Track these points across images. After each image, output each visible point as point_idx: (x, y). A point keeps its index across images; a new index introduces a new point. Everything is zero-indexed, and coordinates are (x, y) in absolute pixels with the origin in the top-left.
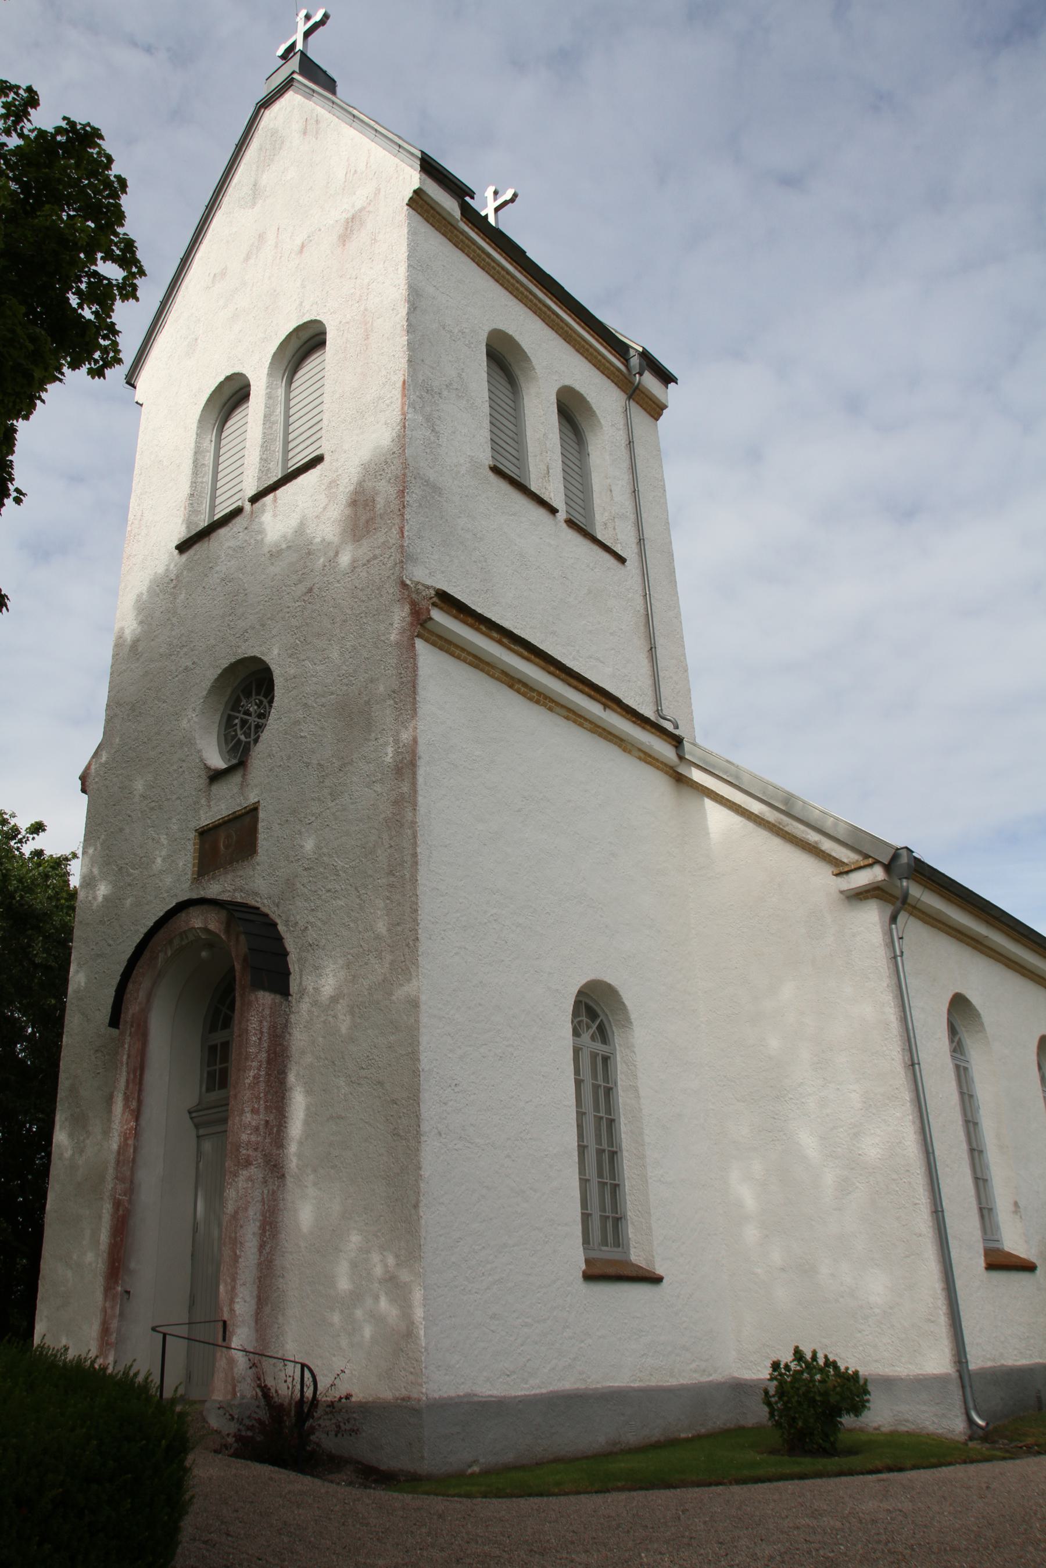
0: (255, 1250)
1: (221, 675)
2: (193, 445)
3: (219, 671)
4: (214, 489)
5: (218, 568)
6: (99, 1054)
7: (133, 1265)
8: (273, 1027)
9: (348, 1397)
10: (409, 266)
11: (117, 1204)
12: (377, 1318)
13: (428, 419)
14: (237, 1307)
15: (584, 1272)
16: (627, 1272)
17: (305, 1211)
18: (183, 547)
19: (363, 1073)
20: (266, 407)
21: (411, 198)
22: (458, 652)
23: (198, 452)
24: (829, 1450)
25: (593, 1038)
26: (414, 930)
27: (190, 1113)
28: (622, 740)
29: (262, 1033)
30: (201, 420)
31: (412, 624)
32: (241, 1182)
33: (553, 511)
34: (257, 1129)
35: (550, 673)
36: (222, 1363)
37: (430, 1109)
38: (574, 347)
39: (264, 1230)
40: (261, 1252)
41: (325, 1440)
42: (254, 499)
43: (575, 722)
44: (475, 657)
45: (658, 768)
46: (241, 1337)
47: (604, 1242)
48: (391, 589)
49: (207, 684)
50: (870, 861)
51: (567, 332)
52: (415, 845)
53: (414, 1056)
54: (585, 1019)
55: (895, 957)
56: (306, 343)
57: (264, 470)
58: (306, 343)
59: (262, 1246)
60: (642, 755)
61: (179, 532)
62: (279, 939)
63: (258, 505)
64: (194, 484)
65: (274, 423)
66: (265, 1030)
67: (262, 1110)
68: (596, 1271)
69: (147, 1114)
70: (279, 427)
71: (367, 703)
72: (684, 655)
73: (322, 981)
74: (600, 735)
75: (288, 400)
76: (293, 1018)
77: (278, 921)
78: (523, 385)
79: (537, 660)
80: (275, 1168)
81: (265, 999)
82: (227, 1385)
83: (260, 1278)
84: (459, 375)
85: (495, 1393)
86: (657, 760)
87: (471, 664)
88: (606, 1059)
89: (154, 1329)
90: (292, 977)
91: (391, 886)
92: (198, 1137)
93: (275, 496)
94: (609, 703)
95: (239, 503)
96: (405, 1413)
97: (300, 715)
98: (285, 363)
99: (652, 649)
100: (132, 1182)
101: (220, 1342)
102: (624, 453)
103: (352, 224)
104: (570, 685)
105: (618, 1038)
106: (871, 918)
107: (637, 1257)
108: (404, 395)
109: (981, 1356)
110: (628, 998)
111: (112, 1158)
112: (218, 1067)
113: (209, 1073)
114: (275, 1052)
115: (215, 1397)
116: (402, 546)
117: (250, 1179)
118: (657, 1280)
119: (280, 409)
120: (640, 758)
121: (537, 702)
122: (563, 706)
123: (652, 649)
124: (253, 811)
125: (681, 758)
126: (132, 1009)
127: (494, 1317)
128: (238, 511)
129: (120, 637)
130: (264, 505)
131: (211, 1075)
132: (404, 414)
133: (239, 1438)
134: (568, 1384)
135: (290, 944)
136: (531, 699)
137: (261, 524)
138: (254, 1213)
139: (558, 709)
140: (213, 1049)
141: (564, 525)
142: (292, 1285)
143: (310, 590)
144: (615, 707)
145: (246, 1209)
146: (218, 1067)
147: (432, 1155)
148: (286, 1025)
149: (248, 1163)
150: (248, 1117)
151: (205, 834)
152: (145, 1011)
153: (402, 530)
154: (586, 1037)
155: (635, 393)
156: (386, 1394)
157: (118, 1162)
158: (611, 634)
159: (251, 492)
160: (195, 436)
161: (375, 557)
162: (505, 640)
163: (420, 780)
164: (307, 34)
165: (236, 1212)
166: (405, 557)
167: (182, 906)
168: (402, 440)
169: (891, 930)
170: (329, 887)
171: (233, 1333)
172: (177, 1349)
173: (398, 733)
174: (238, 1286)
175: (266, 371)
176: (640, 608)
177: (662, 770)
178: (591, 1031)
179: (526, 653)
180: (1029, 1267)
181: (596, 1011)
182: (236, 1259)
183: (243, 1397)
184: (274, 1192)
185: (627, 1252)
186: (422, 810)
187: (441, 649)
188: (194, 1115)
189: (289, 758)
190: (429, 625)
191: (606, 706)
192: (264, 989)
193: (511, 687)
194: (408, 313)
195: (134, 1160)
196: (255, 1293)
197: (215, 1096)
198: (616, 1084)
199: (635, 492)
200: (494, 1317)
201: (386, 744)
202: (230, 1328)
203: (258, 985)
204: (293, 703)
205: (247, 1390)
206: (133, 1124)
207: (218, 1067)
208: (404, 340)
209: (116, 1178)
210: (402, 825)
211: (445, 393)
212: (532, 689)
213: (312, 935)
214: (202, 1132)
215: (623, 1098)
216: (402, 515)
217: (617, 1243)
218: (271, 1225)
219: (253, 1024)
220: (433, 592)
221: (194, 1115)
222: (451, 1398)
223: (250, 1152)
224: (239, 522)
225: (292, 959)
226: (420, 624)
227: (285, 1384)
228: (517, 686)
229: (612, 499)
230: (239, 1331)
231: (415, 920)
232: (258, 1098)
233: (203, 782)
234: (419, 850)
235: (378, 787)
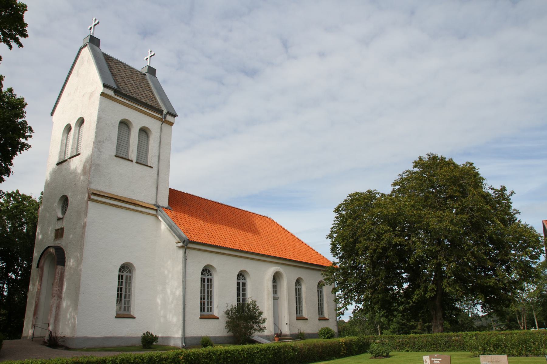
11: (36, 302)
17: (65, 304)
18: (58, 164)
23: (62, 140)
24: (150, 348)
33: (132, 161)
37: (82, 289)
41: (60, 343)
42: (70, 158)
53: (80, 280)
56: (81, 121)
57: (72, 151)
58: (81, 121)
59: (56, 311)
61: (56, 160)
64: (61, 148)
69: (42, 285)
73: (71, 262)
80: (60, 297)
81: (60, 267)
99: (157, 187)
102: (159, 139)
103: (92, 94)
106: (181, 252)
107: (132, 314)
109: (189, 334)
110: (135, 265)
118: (134, 318)
119: (77, 135)
123: (157, 187)
124: (63, 228)
129: (47, 181)
134: (109, 335)
148: (64, 271)
149: (54, 296)
152: (44, 264)
155: (164, 121)
156: (71, 336)
164: (95, 25)
168: (92, 155)
176: (156, 178)
180: (218, 318)
181: (126, 270)
185: (130, 312)
199: (159, 149)
208: (95, 131)
217: (128, 310)
218: (58, 307)
226: (90, 199)
233: (56, 219)
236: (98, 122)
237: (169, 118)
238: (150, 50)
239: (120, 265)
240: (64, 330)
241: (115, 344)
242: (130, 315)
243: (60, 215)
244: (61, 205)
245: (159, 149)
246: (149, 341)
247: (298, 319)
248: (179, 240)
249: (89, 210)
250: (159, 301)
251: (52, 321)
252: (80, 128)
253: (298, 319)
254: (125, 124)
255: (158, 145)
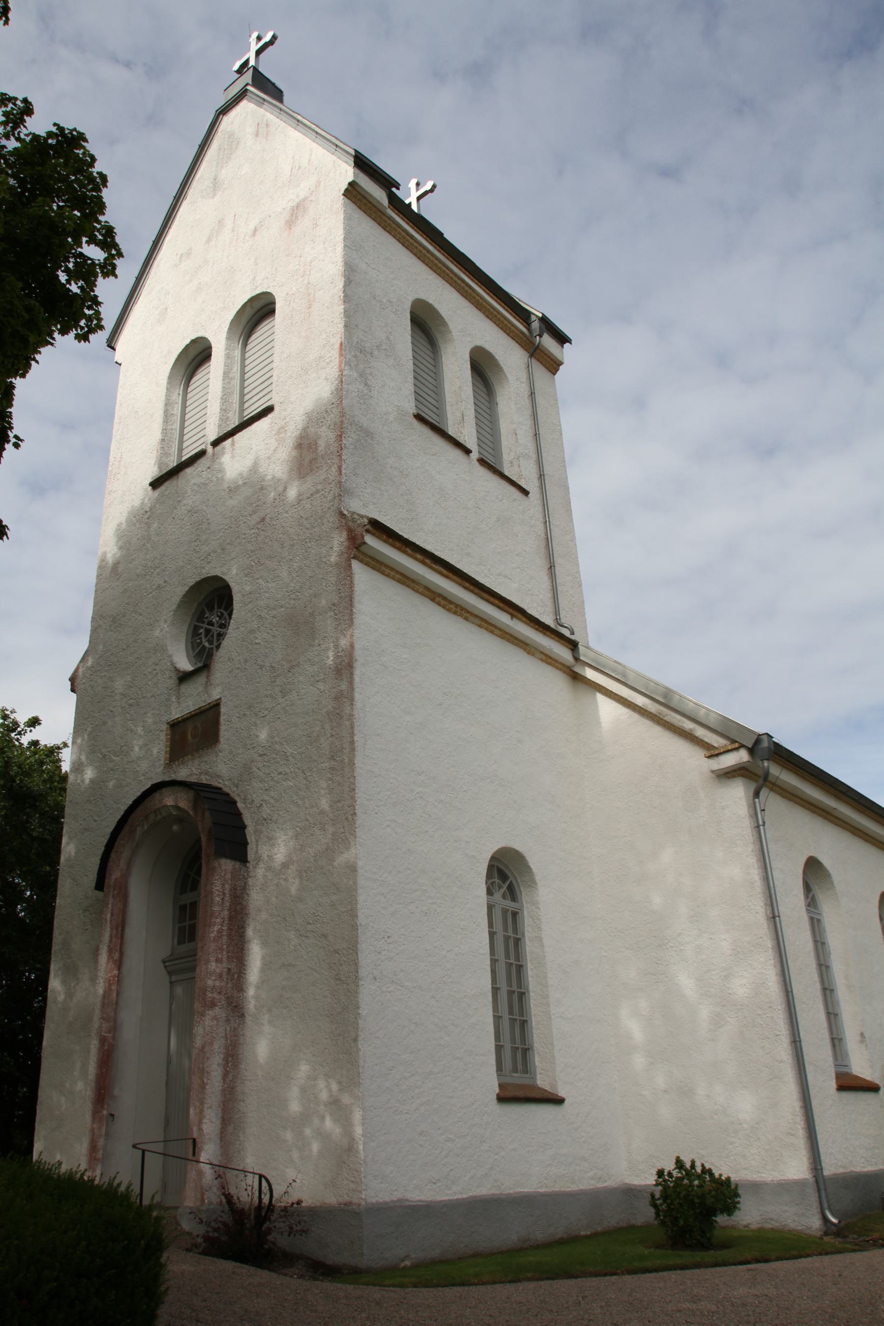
0: (219, 1078)
1: (188, 592)
2: (163, 398)
3: (187, 588)
4: (182, 435)
5: (185, 502)
6: (87, 913)
7: (116, 1092)
8: (234, 889)
9: (299, 1202)
10: (345, 246)
11: (103, 1041)
12: (321, 1135)
13: (362, 375)
14: (204, 1127)
15: (498, 1095)
16: (534, 1095)
17: (262, 1046)
18: (156, 484)
19: (310, 927)
20: (225, 365)
21: (346, 189)
22: (387, 571)
23: (168, 404)
24: (706, 1245)
25: (504, 897)
26: (352, 806)
27: (164, 962)
28: (527, 644)
29: (224, 894)
30: (170, 377)
31: (349, 548)
32: (208, 1021)
33: (467, 451)
34: (221, 975)
35: (465, 588)
36: (192, 1175)
38: (484, 313)
39: (227, 1062)
40: (224, 1080)
41: (280, 1239)
42: (216, 443)
43: (487, 629)
44: (402, 575)
45: (557, 668)
46: (208, 1153)
47: (515, 1070)
48: (332, 519)
49: (177, 599)
50: (737, 745)
51: (478, 301)
52: (352, 734)
53: (353, 913)
54: (496, 880)
55: (758, 827)
56: (259, 311)
57: (223, 419)
58: (259, 311)
59: (225, 1075)
60: (544, 657)
61: (152, 472)
62: (239, 815)
63: (218, 448)
64: (165, 431)
65: (232, 379)
66: (227, 892)
67: (225, 959)
68: (509, 1094)
70: (237, 382)
71: (312, 614)
72: (578, 572)
73: (275, 849)
74: (508, 640)
75: (243, 359)
76: (250, 881)
77: (237, 799)
78: (441, 346)
79: (455, 577)
80: (236, 1008)
81: (227, 865)
82: (197, 1193)
83: (224, 1102)
84: (388, 338)
85: (423, 1198)
86: (556, 661)
87: (399, 581)
88: (515, 914)
89: (134, 1146)
90: (249, 847)
91: (332, 769)
92: (171, 983)
93: (233, 441)
94: (515, 613)
95: (203, 447)
96: (347, 1216)
97: (255, 625)
98: (241, 328)
99: (551, 568)
100: (115, 1021)
101: (191, 1157)
103: (297, 211)
104: (482, 598)
105: (525, 896)
106: (737, 793)
107: (542, 1082)
108: (341, 355)
109: (829, 1169)
110: (533, 862)
111: (99, 1001)
112: (187, 923)
113: (180, 929)
114: (235, 910)
115: (186, 1204)
116: (340, 482)
117: (215, 1018)
118: (559, 1101)
119: (237, 368)
120: (542, 660)
121: (455, 613)
122: (477, 616)
123: (551, 568)
124: (216, 706)
125: (577, 659)
126: (114, 876)
127: (421, 1133)
128: (202, 454)
129: (103, 560)
130: (224, 448)
131: (181, 930)
132: (341, 371)
133: (206, 1238)
134: (484, 1190)
135: (247, 819)
136: (449, 610)
137: (221, 464)
138: (218, 1046)
139: (472, 619)
140: (183, 908)
141: (477, 464)
142: (251, 1107)
143: (263, 520)
144: (520, 616)
145: (211, 1044)
146: (187, 923)
147: (369, 996)
148: (245, 888)
149: (213, 1005)
150: (213, 966)
151: (174, 725)
153: (340, 468)
154: (498, 896)
155: (535, 352)
156: (331, 1199)
157: (103, 1005)
158: (517, 555)
159: (213, 437)
160: (165, 390)
161: (317, 492)
162: (428, 561)
163: (357, 679)
164: (259, 52)
165: (203, 1047)
166: (343, 491)
167: (156, 788)
168: (340, 392)
169: (754, 803)
170: (281, 770)
171: (201, 1149)
172: (154, 1163)
173: (337, 639)
174: (205, 1109)
175: (225, 335)
177: (560, 670)
178: (502, 891)
179: (445, 572)
180: (873, 1088)
181: (506, 874)
182: (203, 1086)
183: (210, 1203)
184: (235, 1029)
185: (534, 1078)
186: (358, 704)
187: (373, 568)
188: (167, 964)
189: (246, 661)
190: (363, 548)
191: (513, 616)
192: (227, 857)
193: (433, 600)
194: (344, 286)
195: (117, 1003)
196: (220, 1115)
197: (185, 948)
198: (523, 935)
199: (536, 435)
200: (421, 1133)
201: (327, 649)
202: (199, 1145)
203: (221, 853)
204: (249, 615)
205: (213, 1197)
206: (116, 972)
207: (187, 923)
209: (102, 1018)
210: (342, 717)
211: (376, 353)
212: (451, 602)
213: (266, 811)
214: (174, 978)
215: (529, 947)
216: (340, 456)
217: (526, 1070)
218: (233, 1057)
219: (217, 887)
220: (366, 521)
221: (167, 964)
222: (386, 1203)
223: (215, 995)
224: (203, 463)
225: (250, 831)
226: (356, 548)
227: (245, 1192)
228: (437, 599)
229: (517, 441)
230: (206, 1147)
231: (353, 798)
232: (221, 949)
233: (173, 682)
234: (356, 738)
235: (321, 686)
236: (348, 282)
237: (548, 342)
238: (413, 182)
239: (488, 856)
240: (289, 1164)
241: (511, 1233)
242: (535, 1087)
243: (185, 664)
244: (185, 628)
245: (536, 435)
246: (691, 1213)
247: (508, 1096)
248: (717, 741)
249: (357, 597)
250: (635, 1029)
251: (210, 1126)
252: (245, 344)
253: (508, 1096)
254: (425, 324)
255: (529, 423)
